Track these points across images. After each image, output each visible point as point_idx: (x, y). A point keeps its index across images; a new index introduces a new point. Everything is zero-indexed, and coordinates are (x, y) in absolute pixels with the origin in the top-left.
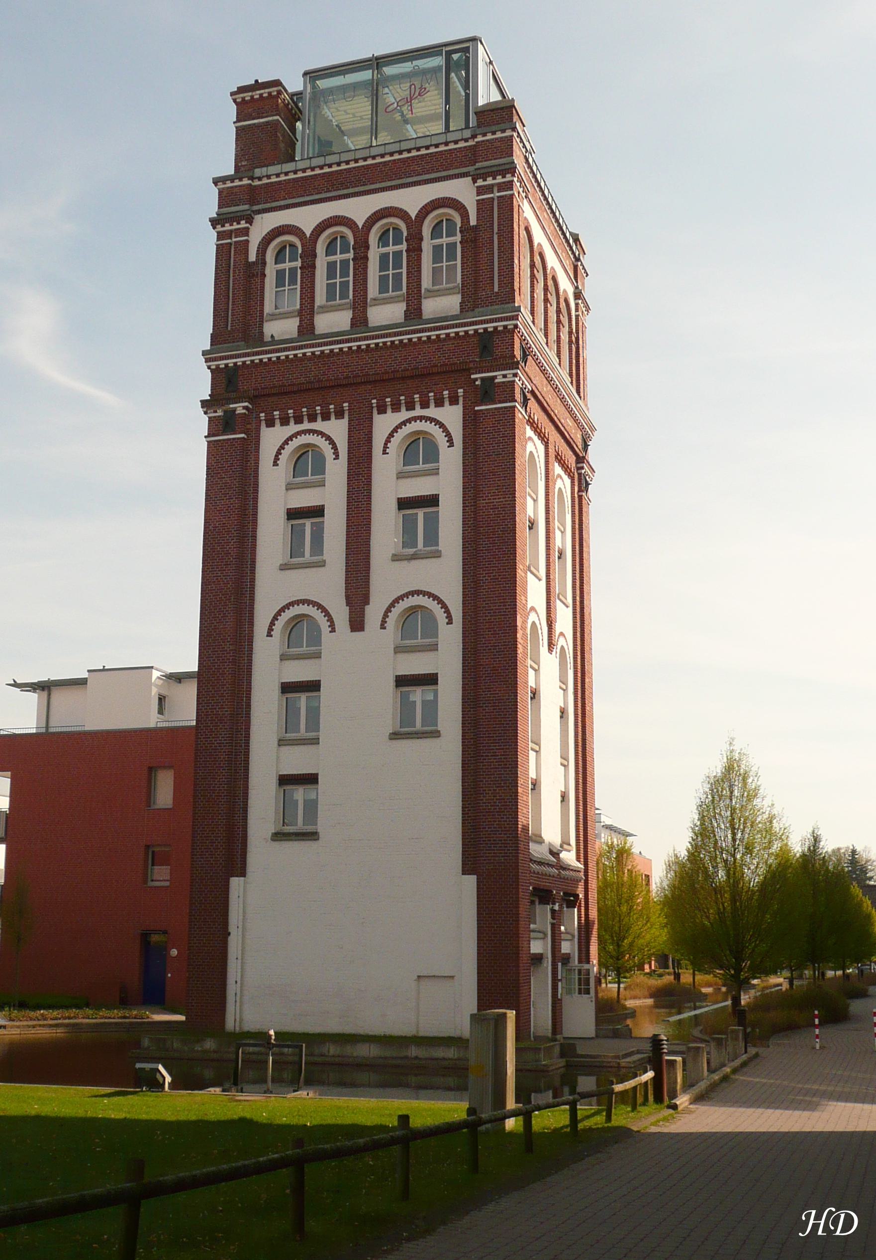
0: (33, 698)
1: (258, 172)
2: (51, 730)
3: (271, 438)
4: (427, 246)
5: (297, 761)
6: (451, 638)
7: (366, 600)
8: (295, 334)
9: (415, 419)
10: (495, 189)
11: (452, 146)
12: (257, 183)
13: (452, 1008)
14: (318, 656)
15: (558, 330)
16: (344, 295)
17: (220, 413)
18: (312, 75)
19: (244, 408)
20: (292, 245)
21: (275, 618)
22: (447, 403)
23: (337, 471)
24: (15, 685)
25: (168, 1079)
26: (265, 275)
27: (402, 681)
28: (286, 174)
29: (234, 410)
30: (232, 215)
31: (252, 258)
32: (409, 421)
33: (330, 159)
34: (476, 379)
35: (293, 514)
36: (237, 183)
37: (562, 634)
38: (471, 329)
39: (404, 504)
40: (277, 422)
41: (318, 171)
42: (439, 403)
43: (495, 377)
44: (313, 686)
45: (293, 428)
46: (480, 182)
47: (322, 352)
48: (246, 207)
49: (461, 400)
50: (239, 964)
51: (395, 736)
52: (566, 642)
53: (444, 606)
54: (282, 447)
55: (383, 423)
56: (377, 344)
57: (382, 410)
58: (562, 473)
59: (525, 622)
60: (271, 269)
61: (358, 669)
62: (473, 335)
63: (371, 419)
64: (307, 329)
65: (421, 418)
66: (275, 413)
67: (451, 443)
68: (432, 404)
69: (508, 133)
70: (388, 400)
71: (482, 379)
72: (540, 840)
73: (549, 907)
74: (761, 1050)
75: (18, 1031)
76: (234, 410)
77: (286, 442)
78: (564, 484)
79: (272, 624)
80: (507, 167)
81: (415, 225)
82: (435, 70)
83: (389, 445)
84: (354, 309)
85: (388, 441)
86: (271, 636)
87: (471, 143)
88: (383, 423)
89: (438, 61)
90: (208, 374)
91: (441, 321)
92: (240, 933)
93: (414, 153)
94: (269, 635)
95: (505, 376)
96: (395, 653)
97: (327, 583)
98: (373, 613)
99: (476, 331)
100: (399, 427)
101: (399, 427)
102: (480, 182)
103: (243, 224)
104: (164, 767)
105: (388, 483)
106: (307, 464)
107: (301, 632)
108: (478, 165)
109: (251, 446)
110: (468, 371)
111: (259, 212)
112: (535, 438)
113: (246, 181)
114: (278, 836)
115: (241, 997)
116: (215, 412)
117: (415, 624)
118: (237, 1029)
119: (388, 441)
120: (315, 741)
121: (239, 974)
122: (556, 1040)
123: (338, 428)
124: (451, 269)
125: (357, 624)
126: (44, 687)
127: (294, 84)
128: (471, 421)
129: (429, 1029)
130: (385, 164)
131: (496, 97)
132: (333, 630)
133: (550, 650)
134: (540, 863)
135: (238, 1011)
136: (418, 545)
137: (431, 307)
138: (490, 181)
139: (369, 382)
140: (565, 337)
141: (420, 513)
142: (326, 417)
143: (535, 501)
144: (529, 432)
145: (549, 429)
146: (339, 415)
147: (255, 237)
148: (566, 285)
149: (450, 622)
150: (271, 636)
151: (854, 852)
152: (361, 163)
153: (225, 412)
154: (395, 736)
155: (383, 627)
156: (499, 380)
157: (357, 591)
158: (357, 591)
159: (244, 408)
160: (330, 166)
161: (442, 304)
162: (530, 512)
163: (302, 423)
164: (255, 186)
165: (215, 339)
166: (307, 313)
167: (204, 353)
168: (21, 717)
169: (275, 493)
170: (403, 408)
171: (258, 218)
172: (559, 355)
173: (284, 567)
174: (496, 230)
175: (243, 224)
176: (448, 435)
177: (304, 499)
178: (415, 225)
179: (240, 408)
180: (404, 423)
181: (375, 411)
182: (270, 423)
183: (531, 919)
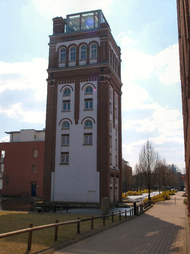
0: (9, 135)
1: (57, 35)
2: (13, 142)
3: (60, 86)
4: (91, 50)
5: (65, 149)
6: (95, 126)
7: (78, 119)
8: (64, 66)
9: (88, 83)
10: (104, 39)
12: (57, 37)
13: (95, 197)
14: (69, 129)
15: (116, 66)
16: (74, 59)
17: (50, 81)
18: (68, 16)
19: (55, 80)
20: (64, 49)
21: (60, 122)
23: (73, 93)
24: (6, 132)
25: (42, 210)
26: (59, 55)
27: (85, 134)
28: (63, 35)
29: (53, 81)
32: (87, 84)
35: (64, 101)
36: (53, 37)
37: (116, 125)
40: (61, 83)
42: (93, 80)
44: (68, 135)
45: (64, 85)
47: (70, 70)
49: (75, 82)
51: (84, 145)
52: (117, 127)
54: (62, 88)
55: (82, 84)
57: (82, 82)
58: (116, 93)
59: (109, 123)
60: (60, 54)
61: (77, 132)
62: (100, 68)
64: (67, 66)
65: (89, 83)
69: (107, 29)
71: (101, 76)
72: (111, 164)
73: (113, 178)
74: (153, 205)
75: (154, 195)
76: (53, 81)
77: (63, 87)
78: (117, 96)
79: (60, 123)
80: (106, 35)
82: (92, 16)
84: (76, 62)
85: (83, 87)
88: (82, 84)
89: (93, 14)
90: (48, 74)
94: (59, 125)
95: (106, 76)
97: (71, 115)
98: (80, 121)
99: (100, 67)
100: (85, 85)
101: (85, 85)
102: (101, 38)
103: (55, 45)
104: (36, 149)
105: (83, 96)
106: (67, 92)
107: (66, 125)
108: (101, 35)
109: (56, 87)
111: (58, 42)
112: (111, 87)
113: (55, 36)
114: (61, 164)
117: (88, 124)
119: (83, 87)
120: (68, 146)
122: (114, 203)
123: (73, 85)
124: (95, 54)
125: (77, 123)
126: (11, 133)
127: (65, 17)
128: (99, 84)
129: (90, 201)
131: (104, 21)
132: (72, 124)
133: (114, 127)
134: (112, 170)
137: (91, 62)
138: (103, 38)
140: (117, 67)
141: (89, 102)
142: (71, 83)
143: (111, 99)
144: (110, 86)
145: (114, 85)
146: (73, 82)
148: (117, 57)
149: (95, 123)
151: (173, 165)
153: (51, 81)
154: (84, 145)
156: (105, 76)
157: (77, 117)
158: (77, 117)
159: (55, 80)
161: (93, 61)
162: (110, 102)
165: (49, 67)
166: (67, 62)
167: (47, 70)
168: (7, 139)
169: (61, 97)
172: (116, 70)
173: (62, 112)
174: (104, 47)
175: (55, 45)
177: (66, 98)
178: (88, 46)
179: (54, 81)
181: (80, 82)
182: (60, 84)
183: (110, 180)
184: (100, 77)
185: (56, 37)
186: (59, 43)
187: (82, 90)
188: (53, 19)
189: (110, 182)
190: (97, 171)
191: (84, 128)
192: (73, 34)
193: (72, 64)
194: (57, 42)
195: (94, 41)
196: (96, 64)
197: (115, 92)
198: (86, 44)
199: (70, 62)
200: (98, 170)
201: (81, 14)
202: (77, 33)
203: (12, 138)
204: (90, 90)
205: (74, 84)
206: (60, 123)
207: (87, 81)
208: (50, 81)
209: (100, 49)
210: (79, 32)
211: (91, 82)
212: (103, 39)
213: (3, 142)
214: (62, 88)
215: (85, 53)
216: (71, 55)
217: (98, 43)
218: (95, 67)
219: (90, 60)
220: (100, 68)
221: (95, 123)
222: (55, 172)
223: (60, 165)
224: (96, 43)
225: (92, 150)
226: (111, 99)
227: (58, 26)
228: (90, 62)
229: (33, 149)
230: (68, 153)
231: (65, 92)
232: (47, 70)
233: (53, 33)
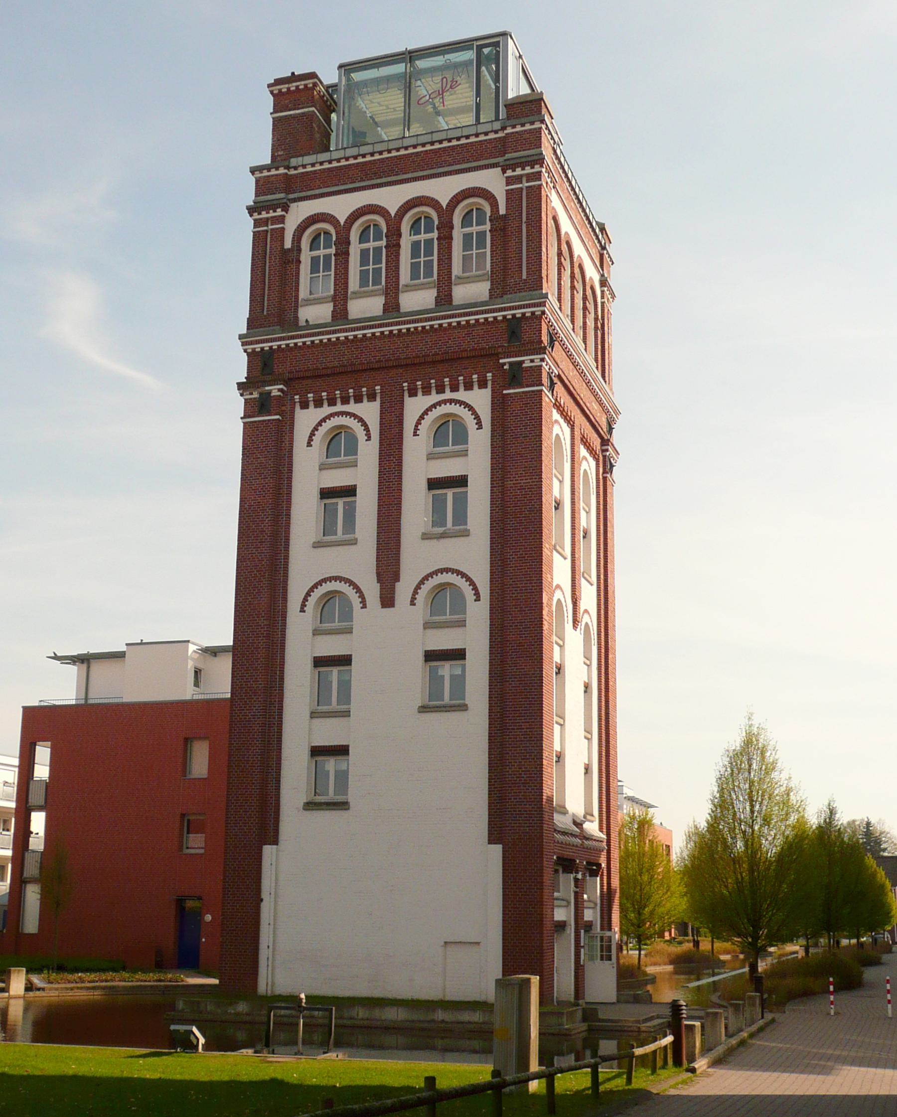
0: (73, 670)
1: (294, 162)
2: (90, 702)
3: (305, 419)
4: (458, 234)
5: (328, 733)
6: (478, 614)
7: (397, 578)
9: (445, 402)
10: (524, 179)
11: (482, 138)
12: (292, 172)
13: (477, 972)
17: (255, 395)
18: (347, 68)
19: (279, 390)
20: (327, 233)
22: (476, 386)
23: (369, 452)
24: (56, 657)
27: (431, 656)
28: (321, 163)
29: (270, 392)
30: (268, 203)
31: (288, 244)
33: (364, 149)
34: (504, 364)
36: (273, 172)
37: (586, 611)
38: (499, 315)
40: (311, 404)
41: (352, 161)
42: (469, 387)
43: (523, 362)
44: (345, 661)
45: (326, 410)
46: (509, 173)
49: (490, 384)
52: (590, 619)
53: (472, 583)
54: (316, 429)
55: (414, 406)
57: (413, 393)
59: (550, 599)
60: (306, 256)
61: (388, 644)
62: (502, 321)
63: (402, 402)
64: (340, 314)
65: (451, 401)
66: (309, 395)
67: (480, 425)
68: (462, 388)
69: (537, 125)
71: (511, 364)
73: (572, 876)
74: (777, 1016)
76: (270, 392)
78: (589, 465)
79: (305, 600)
80: (536, 158)
81: (446, 215)
82: (466, 64)
83: (419, 427)
84: (386, 295)
88: (414, 406)
91: (471, 307)
92: (273, 899)
93: (446, 144)
95: (532, 361)
96: (425, 628)
97: (359, 561)
98: (403, 589)
100: (429, 409)
101: (429, 409)
102: (509, 173)
103: (279, 212)
105: (418, 463)
106: (339, 444)
107: (333, 607)
108: (508, 156)
110: (497, 356)
111: (295, 200)
112: (562, 421)
113: (282, 171)
114: (310, 806)
116: (251, 394)
117: (444, 600)
118: (269, 992)
120: (346, 714)
122: (578, 1005)
123: (370, 411)
125: (388, 601)
126: (84, 660)
127: (329, 76)
128: (499, 404)
131: (525, 90)
132: (364, 606)
133: (575, 622)
134: (564, 833)
136: (447, 525)
137: (461, 293)
138: (519, 171)
141: (450, 493)
142: (358, 399)
144: (556, 415)
145: (575, 413)
146: (372, 397)
149: (478, 599)
150: (304, 611)
153: (261, 394)
155: (413, 603)
156: (527, 364)
159: (279, 390)
161: (472, 291)
162: (556, 492)
167: (241, 337)
169: (308, 472)
170: (434, 391)
171: (293, 206)
172: (585, 340)
173: (317, 545)
175: (279, 212)
177: (337, 479)
179: (275, 390)
180: (434, 406)
181: (406, 394)
182: (305, 405)
183: (555, 887)
184: (506, 367)
187: (415, 434)
189: (556, 894)
190: (491, 841)
192: (368, 158)
194: (291, 196)
195: (433, 199)
197: (582, 447)
199: (358, 295)
200: (493, 839)
202: (389, 151)
203: (87, 683)
204: (447, 433)
206: (305, 600)
207: (440, 390)
209: (503, 228)
211: (462, 395)
212: (521, 176)
213: (42, 704)
214: (316, 429)
216: (359, 264)
217: (493, 197)
218: (514, 316)
220: (504, 325)
221: (478, 599)
223: (304, 809)
224: (486, 199)
225: (469, 734)
226: (561, 482)
228: (453, 294)
229: (186, 740)
232: (241, 337)
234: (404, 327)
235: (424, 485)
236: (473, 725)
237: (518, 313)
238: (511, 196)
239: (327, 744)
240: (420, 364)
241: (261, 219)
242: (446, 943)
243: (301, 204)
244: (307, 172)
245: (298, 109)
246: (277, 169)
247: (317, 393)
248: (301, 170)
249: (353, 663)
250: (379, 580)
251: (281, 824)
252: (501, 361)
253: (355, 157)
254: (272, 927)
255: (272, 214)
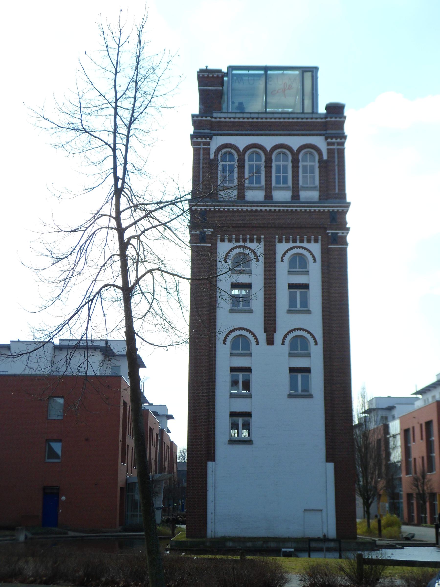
1: (215, 115)
5: (240, 406)
6: (317, 353)
9: (297, 247)
10: (336, 145)
11: (314, 120)
12: (213, 120)
17: (198, 233)
19: (211, 231)
22: (312, 241)
23: (258, 269)
27: (292, 370)
29: (205, 232)
30: (203, 135)
31: (212, 157)
33: (245, 115)
34: (329, 233)
36: (200, 118)
38: (326, 209)
39: (291, 286)
41: (246, 120)
42: (309, 241)
46: (329, 140)
48: (209, 131)
49: (320, 241)
50: (213, 504)
53: (313, 336)
55: (281, 248)
56: (279, 210)
57: (280, 241)
61: (270, 364)
62: (318, 212)
63: (275, 245)
65: (300, 247)
66: (226, 236)
67: (315, 261)
68: (305, 241)
70: (284, 236)
71: (332, 233)
81: (241, 155)
83: (284, 258)
84: (266, 190)
86: (225, 344)
87: (323, 120)
91: (310, 203)
92: (213, 489)
93: (295, 120)
95: (343, 233)
96: (289, 356)
97: (255, 321)
98: (278, 337)
103: (208, 140)
105: (283, 277)
107: (241, 344)
109: (214, 249)
110: (326, 229)
111: (216, 135)
113: (209, 118)
115: (215, 519)
116: (196, 232)
117: (299, 345)
118: (213, 536)
121: (213, 509)
123: (258, 247)
125: (270, 342)
127: (225, 70)
128: (325, 252)
130: (285, 122)
132: (258, 344)
135: (213, 527)
136: (299, 307)
137: (304, 195)
138: (334, 140)
139: (275, 227)
147: (213, 147)
149: (316, 344)
150: (225, 344)
152: (268, 120)
153: (201, 232)
155: (283, 344)
157: (270, 326)
158: (270, 326)
160: (253, 118)
161: (310, 195)
163: (239, 242)
164: (213, 121)
170: (291, 241)
171: (214, 137)
176: (313, 256)
178: (241, 155)
179: (209, 231)
181: (277, 241)
182: (222, 240)
184: (330, 234)
185: (210, 120)
186: (219, 137)
187: (282, 261)
188: (198, 72)
191: (231, 355)
193: (282, 195)
196: (235, 202)
198: (235, 148)
201: (266, 69)
205: (262, 244)
208: (198, 233)
210: (299, 116)
215: (232, 171)
219: (301, 190)
221: (316, 344)
222: (217, 460)
223: (229, 444)
227: (211, 90)
230: (249, 414)
231: (292, 263)
233: (200, 109)
234: (277, 209)
235: (287, 286)
236: (317, 405)
237: (336, 209)
238: (330, 152)
239: (238, 411)
240: (285, 228)
241: (197, 142)
242: (305, 510)
243: (218, 137)
244: (221, 121)
245: (214, 87)
246: (202, 117)
247: (230, 235)
248: (218, 120)
249: (252, 371)
250: (265, 331)
251: (216, 451)
252: (328, 231)
253: (248, 118)
254: (213, 503)
255: (204, 140)
